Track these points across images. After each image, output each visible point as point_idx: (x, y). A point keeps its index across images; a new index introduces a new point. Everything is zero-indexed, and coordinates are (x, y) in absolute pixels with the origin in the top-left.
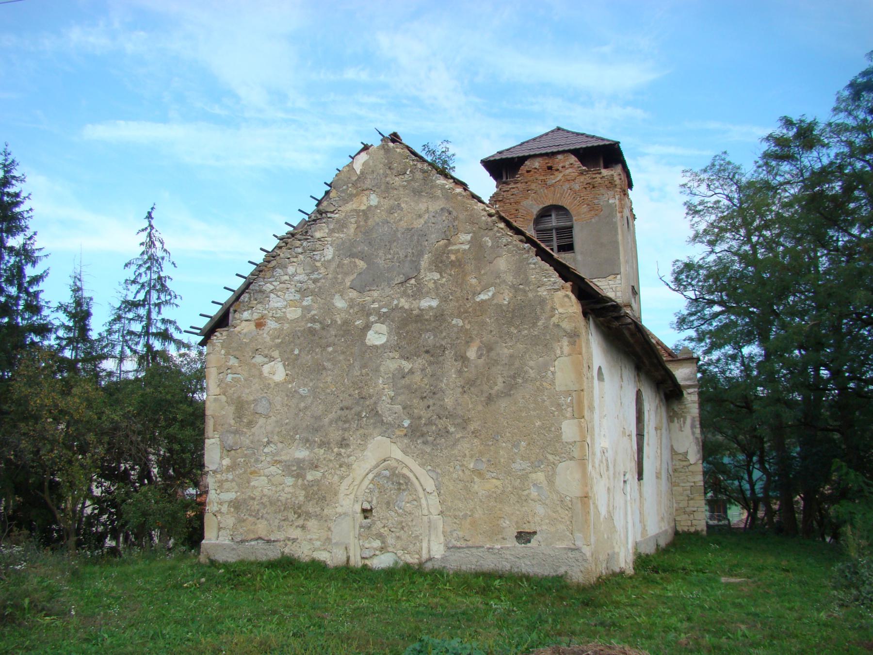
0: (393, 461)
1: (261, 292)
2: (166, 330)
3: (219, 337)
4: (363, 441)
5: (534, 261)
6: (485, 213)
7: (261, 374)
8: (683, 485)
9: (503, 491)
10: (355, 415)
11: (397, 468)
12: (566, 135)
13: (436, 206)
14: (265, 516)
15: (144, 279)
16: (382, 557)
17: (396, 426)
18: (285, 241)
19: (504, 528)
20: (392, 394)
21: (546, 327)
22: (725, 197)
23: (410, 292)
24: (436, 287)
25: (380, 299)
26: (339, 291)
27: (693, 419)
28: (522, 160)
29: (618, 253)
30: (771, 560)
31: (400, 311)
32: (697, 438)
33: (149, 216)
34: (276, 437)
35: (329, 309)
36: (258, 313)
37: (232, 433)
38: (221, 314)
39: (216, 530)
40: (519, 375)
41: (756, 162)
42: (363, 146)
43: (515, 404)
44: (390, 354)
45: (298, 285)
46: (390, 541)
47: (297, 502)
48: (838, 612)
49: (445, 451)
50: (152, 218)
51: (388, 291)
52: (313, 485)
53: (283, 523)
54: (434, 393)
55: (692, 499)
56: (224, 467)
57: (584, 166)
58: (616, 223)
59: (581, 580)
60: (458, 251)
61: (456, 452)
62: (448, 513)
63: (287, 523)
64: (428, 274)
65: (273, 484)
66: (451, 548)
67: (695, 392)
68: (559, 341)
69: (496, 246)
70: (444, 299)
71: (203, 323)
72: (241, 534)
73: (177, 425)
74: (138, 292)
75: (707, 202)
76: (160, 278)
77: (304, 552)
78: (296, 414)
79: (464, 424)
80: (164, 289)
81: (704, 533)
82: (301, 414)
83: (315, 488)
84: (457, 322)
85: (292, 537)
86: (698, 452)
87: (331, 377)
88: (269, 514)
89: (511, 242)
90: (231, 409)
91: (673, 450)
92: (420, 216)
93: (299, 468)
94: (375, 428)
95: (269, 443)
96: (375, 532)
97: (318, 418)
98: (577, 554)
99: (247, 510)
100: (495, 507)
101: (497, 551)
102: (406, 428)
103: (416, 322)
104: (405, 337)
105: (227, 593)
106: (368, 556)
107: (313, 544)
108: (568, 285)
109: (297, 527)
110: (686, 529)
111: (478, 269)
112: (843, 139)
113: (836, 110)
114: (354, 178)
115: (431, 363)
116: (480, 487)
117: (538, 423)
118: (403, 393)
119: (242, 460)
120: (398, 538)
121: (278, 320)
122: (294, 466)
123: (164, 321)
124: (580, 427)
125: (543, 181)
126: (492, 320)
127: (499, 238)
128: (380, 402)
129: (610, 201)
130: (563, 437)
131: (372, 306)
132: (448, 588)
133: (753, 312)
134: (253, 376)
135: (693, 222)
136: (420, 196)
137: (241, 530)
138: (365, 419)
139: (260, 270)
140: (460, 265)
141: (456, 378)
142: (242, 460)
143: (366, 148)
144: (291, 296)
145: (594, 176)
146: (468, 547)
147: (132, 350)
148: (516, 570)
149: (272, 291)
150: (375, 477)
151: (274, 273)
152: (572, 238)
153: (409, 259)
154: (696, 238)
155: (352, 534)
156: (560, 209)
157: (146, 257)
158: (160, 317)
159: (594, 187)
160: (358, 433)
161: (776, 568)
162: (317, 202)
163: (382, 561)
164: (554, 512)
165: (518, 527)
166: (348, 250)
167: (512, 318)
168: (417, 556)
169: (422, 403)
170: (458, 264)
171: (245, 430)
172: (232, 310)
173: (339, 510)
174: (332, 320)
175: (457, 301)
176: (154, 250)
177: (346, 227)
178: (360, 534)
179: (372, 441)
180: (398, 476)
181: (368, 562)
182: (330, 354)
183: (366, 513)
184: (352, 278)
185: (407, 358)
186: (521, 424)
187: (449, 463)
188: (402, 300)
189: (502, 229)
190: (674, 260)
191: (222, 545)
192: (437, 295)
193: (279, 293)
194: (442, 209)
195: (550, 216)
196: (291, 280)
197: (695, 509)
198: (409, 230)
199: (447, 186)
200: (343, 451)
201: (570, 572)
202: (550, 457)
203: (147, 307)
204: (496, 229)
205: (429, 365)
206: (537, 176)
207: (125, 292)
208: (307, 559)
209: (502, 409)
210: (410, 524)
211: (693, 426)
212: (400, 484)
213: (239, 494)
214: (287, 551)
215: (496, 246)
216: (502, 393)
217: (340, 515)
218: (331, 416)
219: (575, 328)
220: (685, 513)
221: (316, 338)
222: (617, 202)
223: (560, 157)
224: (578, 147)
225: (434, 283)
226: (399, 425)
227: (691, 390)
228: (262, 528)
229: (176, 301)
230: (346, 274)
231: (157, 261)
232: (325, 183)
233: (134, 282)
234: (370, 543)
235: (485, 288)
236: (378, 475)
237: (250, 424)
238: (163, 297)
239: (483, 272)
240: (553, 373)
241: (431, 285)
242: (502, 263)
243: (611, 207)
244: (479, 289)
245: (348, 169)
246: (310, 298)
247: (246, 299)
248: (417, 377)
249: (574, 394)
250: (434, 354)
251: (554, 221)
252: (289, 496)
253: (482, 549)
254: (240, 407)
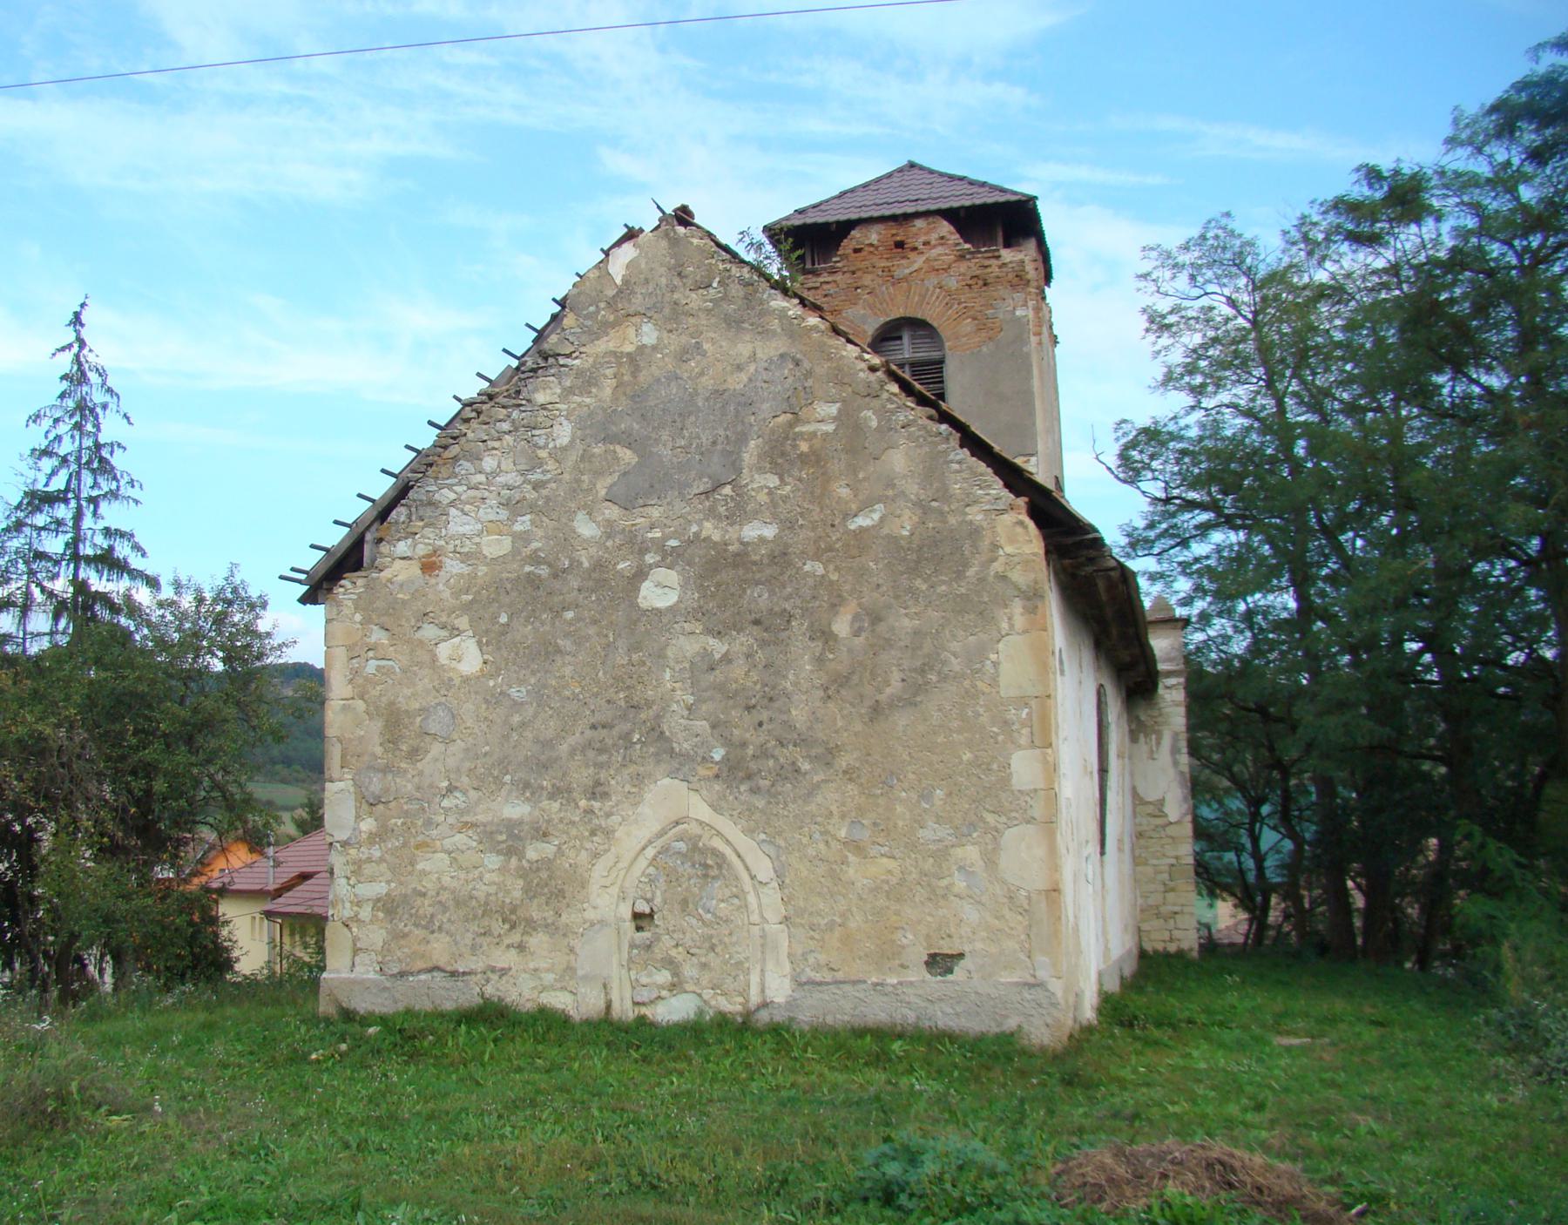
0: (694, 824)
1: (432, 504)
2: (111, 549)
3: (349, 589)
4: (635, 786)
5: (958, 457)
6: (863, 365)
7: (434, 659)
8: (1155, 862)
9: (903, 880)
10: (620, 738)
11: (700, 837)
12: (929, 178)
13: (770, 349)
14: (446, 926)
15: (66, 447)
16: (673, 1000)
17: (699, 759)
18: (472, 410)
19: (903, 947)
20: (690, 699)
21: (982, 580)
22: (1224, 300)
23: (722, 510)
24: (772, 501)
25: (665, 521)
26: (585, 507)
27: (1175, 736)
28: (846, 227)
29: (1032, 414)
30: (1339, 1005)
31: (703, 544)
32: (1182, 773)
33: (77, 320)
34: (465, 779)
35: (567, 540)
36: (426, 544)
37: (379, 770)
38: (348, 544)
39: (349, 954)
40: (931, 669)
41: (1285, 233)
42: (626, 230)
43: (925, 720)
44: (686, 625)
45: (503, 492)
46: (689, 971)
47: (508, 901)
48: (1519, 1093)
49: (791, 806)
50: (82, 325)
51: (680, 507)
52: (538, 869)
53: (482, 939)
54: (771, 699)
55: (1173, 890)
56: (364, 836)
57: (966, 242)
58: (1028, 355)
59: (1046, 1041)
60: (814, 434)
61: (812, 807)
62: (798, 920)
63: (488, 939)
64: (756, 476)
65: (461, 868)
66: (805, 983)
67: (1179, 684)
68: (1006, 606)
69: (886, 429)
70: (788, 525)
71: (311, 560)
72: (400, 960)
73: (158, 745)
74: (54, 473)
75: (1186, 309)
76: (98, 446)
77: (522, 993)
78: (503, 736)
79: (828, 756)
80: (105, 468)
81: (1195, 954)
82: (515, 736)
83: (544, 875)
84: (814, 567)
85: (500, 965)
86: (1185, 799)
87: (572, 668)
88: (453, 922)
89: (915, 421)
90: (377, 726)
91: (1135, 793)
92: (739, 368)
93: (511, 836)
94: (658, 762)
95: (451, 789)
96: (659, 956)
97: (548, 744)
98: (1039, 994)
99: (411, 915)
100: (888, 908)
101: (891, 989)
102: (717, 763)
103: (735, 566)
104: (713, 596)
105: (397, 1074)
106: (646, 1000)
107: (540, 978)
108: (1022, 502)
109: (508, 946)
110: (1160, 947)
111: (853, 470)
112: (1466, 199)
113: (1452, 142)
114: (611, 292)
115: (763, 644)
116: (858, 873)
117: (967, 756)
118: (711, 699)
119: (399, 822)
120: (704, 966)
121: (466, 557)
122: (501, 833)
123: (107, 532)
124: (1045, 762)
125: (888, 270)
126: (880, 566)
127: (893, 412)
128: (668, 715)
129: (1018, 313)
130: (1014, 780)
131: (650, 535)
132: (809, 1055)
133: (1271, 525)
134: (420, 664)
135: (1157, 348)
136: (740, 329)
137: (399, 954)
138: (638, 746)
139: (425, 463)
140: (818, 462)
141: (812, 671)
142: (399, 822)
143: (631, 235)
144: (490, 512)
145: (987, 263)
146: (837, 982)
147: (43, 590)
148: (927, 1023)
149: (452, 504)
150: (659, 853)
151: (457, 470)
152: (942, 382)
153: (719, 447)
154: (1169, 379)
155: (615, 960)
156: (917, 325)
157: (70, 403)
158: (101, 524)
159: (985, 285)
160: (626, 772)
161: (1359, 1019)
162: (535, 334)
163: (673, 1010)
164: (997, 918)
165: (930, 946)
166: (600, 429)
167: (918, 562)
168: (741, 1000)
169: (746, 716)
170: (814, 459)
171: (403, 765)
172: (368, 537)
173: (591, 915)
174: (572, 560)
175: (814, 529)
176: (85, 389)
177: (596, 385)
178: (630, 960)
179: (652, 787)
180: (703, 851)
181: (644, 1010)
182: (570, 623)
183: (641, 919)
184: (609, 480)
185: (719, 633)
186: (935, 758)
187: (801, 828)
188: (707, 525)
189: (895, 395)
190: (1118, 419)
191: (361, 982)
192: (775, 516)
193: (467, 508)
194: (782, 356)
195: (900, 338)
196: (489, 483)
197: (1177, 909)
198: (719, 393)
199: (790, 313)
200: (596, 805)
201: (1025, 1026)
202: (990, 818)
203: (73, 504)
204: (885, 396)
205: (760, 646)
206: (875, 260)
207: (31, 474)
208: (529, 1006)
209: (900, 728)
210: (726, 939)
211: (1175, 751)
212: (706, 866)
213: (393, 885)
214: (489, 990)
215: (886, 429)
216: (900, 699)
217: (592, 925)
218: (573, 740)
219: (1036, 583)
220: (1158, 916)
221: (541, 592)
222: (1031, 314)
223: (920, 223)
224: (956, 205)
225: (768, 494)
226: (704, 758)
227: (1172, 681)
228: (439, 949)
229: (134, 493)
230: (599, 474)
231: (92, 411)
232: (554, 300)
233: (47, 452)
234: (650, 975)
235: (866, 506)
236: (665, 850)
237: (414, 754)
238: (106, 485)
239: (861, 476)
240: (996, 664)
241: (763, 497)
242: (899, 460)
243: (1020, 323)
244: (854, 507)
245: (597, 273)
246: (528, 517)
247: (402, 518)
248: (738, 670)
249: (1033, 703)
250: (770, 626)
251: (907, 349)
252: (492, 890)
253: (864, 986)
254: (394, 722)
